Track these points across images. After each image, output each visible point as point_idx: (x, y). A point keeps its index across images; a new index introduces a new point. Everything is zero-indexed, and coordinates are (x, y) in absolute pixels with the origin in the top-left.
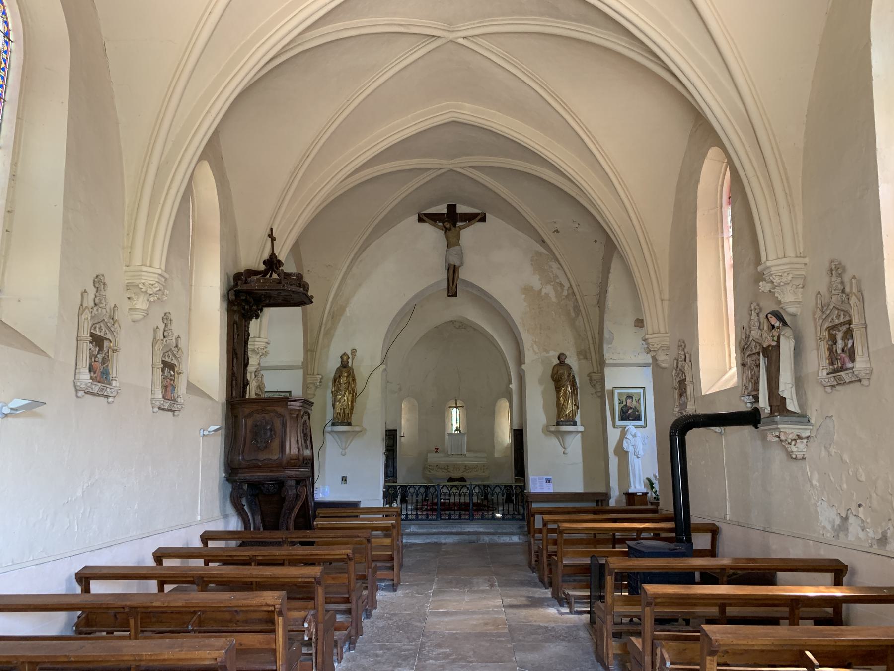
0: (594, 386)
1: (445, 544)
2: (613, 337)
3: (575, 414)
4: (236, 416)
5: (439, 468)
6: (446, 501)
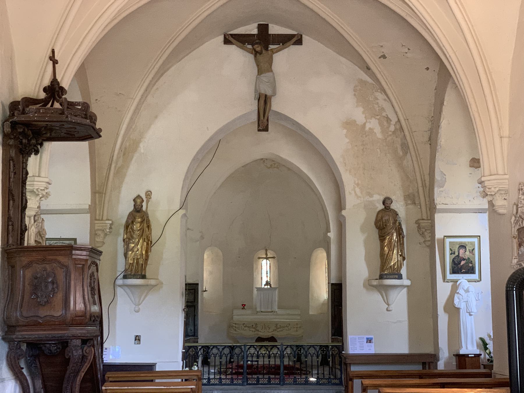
0: (423, 235)
2: (445, 178)
3: (401, 266)
4: (13, 267)
6: (254, 363)
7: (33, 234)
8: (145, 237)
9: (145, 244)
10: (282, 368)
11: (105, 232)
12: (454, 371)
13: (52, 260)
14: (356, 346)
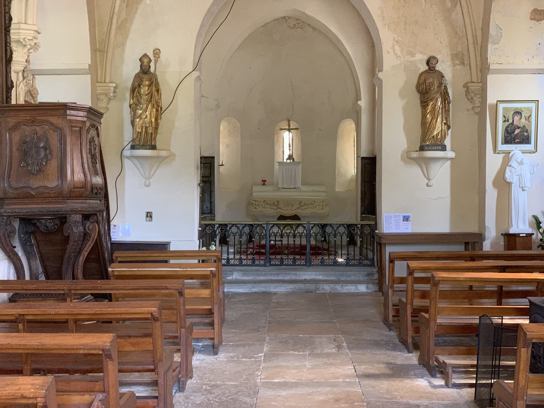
0: (471, 100)
1: (275, 294)
2: (501, 33)
3: (445, 136)
5: (267, 204)
6: (277, 243)
7: (22, 92)
8: (154, 103)
9: (155, 111)
10: (308, 249)
11: (109, 97)
12: (501, 253)
13: (43, 121)
14: (392, 225)
